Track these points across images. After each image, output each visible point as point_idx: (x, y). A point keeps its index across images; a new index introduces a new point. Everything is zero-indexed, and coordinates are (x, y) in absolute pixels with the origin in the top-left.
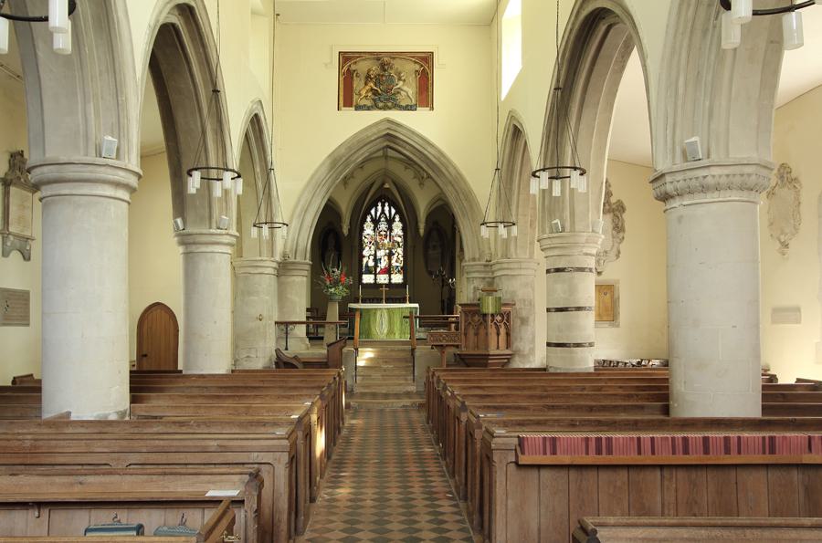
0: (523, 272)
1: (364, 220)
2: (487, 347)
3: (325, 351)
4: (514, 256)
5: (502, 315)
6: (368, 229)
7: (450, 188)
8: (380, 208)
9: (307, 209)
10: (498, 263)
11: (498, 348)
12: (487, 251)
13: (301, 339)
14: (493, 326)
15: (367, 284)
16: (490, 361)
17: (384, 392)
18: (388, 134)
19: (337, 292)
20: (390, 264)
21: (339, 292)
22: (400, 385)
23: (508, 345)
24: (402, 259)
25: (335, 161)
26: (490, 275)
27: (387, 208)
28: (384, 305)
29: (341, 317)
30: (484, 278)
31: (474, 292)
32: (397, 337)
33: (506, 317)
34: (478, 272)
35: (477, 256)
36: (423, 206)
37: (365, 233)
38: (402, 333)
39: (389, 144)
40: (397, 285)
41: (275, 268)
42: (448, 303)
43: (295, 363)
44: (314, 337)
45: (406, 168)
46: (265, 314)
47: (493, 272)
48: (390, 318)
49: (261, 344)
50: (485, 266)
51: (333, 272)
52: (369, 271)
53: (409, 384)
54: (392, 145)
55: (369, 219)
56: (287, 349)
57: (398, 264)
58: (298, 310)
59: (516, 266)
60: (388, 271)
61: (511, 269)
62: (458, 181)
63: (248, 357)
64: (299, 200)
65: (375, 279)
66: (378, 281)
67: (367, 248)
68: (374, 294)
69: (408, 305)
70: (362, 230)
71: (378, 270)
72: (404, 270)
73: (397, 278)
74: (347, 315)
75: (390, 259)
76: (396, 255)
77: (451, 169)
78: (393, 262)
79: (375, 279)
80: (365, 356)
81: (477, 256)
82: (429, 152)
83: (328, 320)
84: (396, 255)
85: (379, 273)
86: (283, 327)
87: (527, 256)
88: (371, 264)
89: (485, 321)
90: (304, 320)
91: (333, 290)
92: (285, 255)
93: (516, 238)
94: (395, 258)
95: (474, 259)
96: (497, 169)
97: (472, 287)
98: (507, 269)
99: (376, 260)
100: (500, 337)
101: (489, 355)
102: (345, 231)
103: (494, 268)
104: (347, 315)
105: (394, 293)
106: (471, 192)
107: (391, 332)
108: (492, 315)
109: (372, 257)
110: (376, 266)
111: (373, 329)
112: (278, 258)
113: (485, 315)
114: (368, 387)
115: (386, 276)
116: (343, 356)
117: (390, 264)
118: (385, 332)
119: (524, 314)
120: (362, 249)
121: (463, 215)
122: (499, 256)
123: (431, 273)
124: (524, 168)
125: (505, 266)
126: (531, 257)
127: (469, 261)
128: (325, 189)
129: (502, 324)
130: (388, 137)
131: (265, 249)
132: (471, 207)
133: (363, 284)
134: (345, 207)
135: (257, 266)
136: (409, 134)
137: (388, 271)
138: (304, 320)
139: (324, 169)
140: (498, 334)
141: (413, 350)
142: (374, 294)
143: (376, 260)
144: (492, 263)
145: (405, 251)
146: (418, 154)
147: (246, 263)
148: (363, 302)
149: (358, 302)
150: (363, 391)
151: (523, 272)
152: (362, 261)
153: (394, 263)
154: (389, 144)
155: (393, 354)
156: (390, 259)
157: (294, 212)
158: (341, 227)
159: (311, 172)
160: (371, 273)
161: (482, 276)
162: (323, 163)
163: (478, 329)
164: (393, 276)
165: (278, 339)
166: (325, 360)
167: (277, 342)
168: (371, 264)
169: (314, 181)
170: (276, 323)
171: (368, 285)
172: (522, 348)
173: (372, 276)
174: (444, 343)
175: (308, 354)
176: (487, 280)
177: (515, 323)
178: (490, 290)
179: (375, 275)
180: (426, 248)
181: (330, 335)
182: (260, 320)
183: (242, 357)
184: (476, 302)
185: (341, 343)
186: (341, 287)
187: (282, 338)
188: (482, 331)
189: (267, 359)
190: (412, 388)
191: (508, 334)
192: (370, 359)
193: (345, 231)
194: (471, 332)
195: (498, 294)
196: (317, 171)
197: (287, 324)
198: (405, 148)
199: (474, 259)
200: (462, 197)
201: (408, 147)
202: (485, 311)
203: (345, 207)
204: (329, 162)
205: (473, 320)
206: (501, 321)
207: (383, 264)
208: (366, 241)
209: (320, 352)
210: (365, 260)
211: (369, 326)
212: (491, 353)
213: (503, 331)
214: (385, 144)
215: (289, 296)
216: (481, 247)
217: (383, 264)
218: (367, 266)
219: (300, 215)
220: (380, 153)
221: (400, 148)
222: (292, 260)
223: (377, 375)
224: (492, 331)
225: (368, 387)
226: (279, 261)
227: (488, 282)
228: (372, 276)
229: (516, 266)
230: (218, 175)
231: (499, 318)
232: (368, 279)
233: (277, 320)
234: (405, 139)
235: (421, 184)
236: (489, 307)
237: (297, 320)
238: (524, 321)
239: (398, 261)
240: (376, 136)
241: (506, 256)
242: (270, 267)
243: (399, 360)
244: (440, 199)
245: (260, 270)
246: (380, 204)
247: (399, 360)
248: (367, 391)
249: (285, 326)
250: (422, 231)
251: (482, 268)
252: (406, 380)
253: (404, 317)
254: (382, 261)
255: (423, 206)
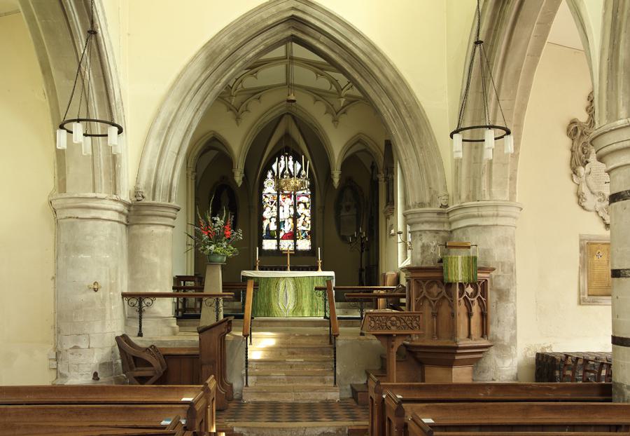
0: (500, 221)
1: (264, 177)
2: (453, 333)
3: (197, 339)
4: (488, 198)
5: (474, 285)
6: (269, 188)
7: (386, 100)
8: (282, 162)
9: (171, 125)
10: (461, 208)
11: (469, 336)
12: (441, 193)
13: (164, 320)
14: (462, 302)
15: (268, 251)
16: (457, 358)
17: (290, 401)
18: (293, 18)
19: (218, 250)
20: (295, 228)
21: (223, 251)
22: (314, 390)
23: (484, 332)
24: (309, 222)
25: (215, 56)
26: (446, 227)
27: (291, 163)
28: (289, 274)
29: (226, 287)
30: (437, 232)
31: (423, 252)
32: (307, 315)
33: (481, 288)
34: (427, 222)
35: (427, 199)
36: (337, 148)
37: (265, 192)
38: (314, 310)
39: (294, 33)
40: (304, 253)
41: (121, 213)
42: (369, 271)
43: (147, 357)
44: (185, 314)
45: (316, 100)
46: (103, 281)
47: (450, 223)
48: (296, 287)
49: (97, 328)
50: (439, 213)
51: (215, 222)
52: (270, 236)
53: (328, 389)
54: (300, 35)
55: (270, 175)
56: (140, 335)
57: (304, 228)
58: (158, 275)
59: (490, 211)
60: (293, 236)
61: (482, 216)
62: (397, 90)
63: (75, 347)
64: (159, 112)
65: (278, 245)
66: (282, 248)
67: (268, 209)
68: (277, 260)
69: (320, 273)
70: (262, 187)
71: (282, 234)
72: (312, 235)
73: (304, 245)
74: (235, 286)
75: (295, 222)
76: (303, 217)
77: (387, 71)
78: (299, 225)
79: (278, 245)
80: (261, 345)
81: (427, 199)
82: (355, 45)
83: (206, 291)
84: (303, 217)
85: (282, 239)
86: (134, 301)
87: (507, 197)
88: (273, 227)
89: (451, 295)
90: (170, 290)
91: (212, 247)
92: (137, 193)
93: (491, 162)
94: (300, 221)
95: (422, 205)
96: (478, 43)
97: (420, 244)
98: (478, 216)
99: (279, 224)
100: (472, 320)
101: (457, 348)
102: (238, 178)
103: (452, 216)
104: (235, 286)
105: (302, 261)
106: (416, 105)
107: (298, 307)
108: (461, 285)
109: (274, 220)
110: (279, 230)
111: (274, 304)
112: (125, 196)
113: (450, 285)
114: (265, 393)
115: (291, 242)
116: (227, 347)
117: (295, 228)
118: (291, 307)
119: (503, 283)
120: (262, 210)
121: (405, 139)
122: (464, 196)
123: (344, 238)
124: (509, 55)
125: (474, 212)
126: (512, 198)
127: (414, 207)
128: (198, 97)
129: (475, 300)
130: (293, 23)
131: (103, 180)
132: (417, 127)
133: (262, 251)
134: (237, 141)
135: (89, 208)
136: (324, 17)
137: (293, 236)
138: (170, 290)
139: (198, 66)
140: (469, 315)
141: (332, 338)
142: (277, 260)
143: (279, 224)
144: (451, 207)
145: (313, 213)
146: (338, 49)
147: (71, 202)
148: (262, 269)
149: (254, 269)
150: (259, 399)
151: (500, 221)
152: (262, 224)
153: (300, 227)
154: (294, 33)
155: (303, 341)
156: (295, 222)
157: (150, 130)
158: (233, 174)
159: (177, 70)
160: (272, 238)
161: (435, 228)
162: (195, 57)
163: (438, 306)
164: (292, 248)
165: (127, 319)
166: (198, 352)
167: (126, 325)
168: (273, 227)
169: (181, 83)
170: (124, 295)
171: (270, 252)
172: (500, 336)
173: (275, 242)
174: (394, 331)
175: (174, 342)
176: (442, 234)
177: (492, 296)
178: (449, 244)
179: (278, 240)
180: (338, 209)
181: (208, 317)
182: (96, 290)
183: (65, 347)
184: (438, 265)
185: (223, 328)
186: (225, 244)
187: (134, 318)
188: (444, 310)
189: (107, 350)
190: (334, 395)
191: (484, 316)
192: (271, 349)
193: (238, 178)
194: (427, 311)
195: (471, 252)
196: (187, 67)
197: (141, 297)
198: (318, 40)
199: (422, 205)
200: (403, 111)
201: (323, 38)
202: (452, 278)
203: (237, 141)
204: (202, 56)
205: (429, 293)
206: (474, 295)
207: (287, 228)
208: (267, 200)
209: (189, 338)
210: (265, 223)
211: (269, 300)
212: (461, 344)
213: (476, 309)
214: (289, 33)
215: (144, 255)
216: (433, 185)
217: (287, 228)
218: (268, 229)
219: (160, 135)
220: (280, 52)
221: (314, 42)
222: (148, 200)
223: (279, 374)
224: (461, 309)
225: (265, 393)
226: (128, 200)
227: (443, 237)
228: (275, 242)
229: (490, 211)
230: (103, 129)
231: (470, 290)
232: (269, 245)
233: (125, 291)
234: (318, 24)
235: (335, 121)
236: (458, 274)
237: (157, 291)
238: (503, 295)
239: (304, 225)
240: (274, 20)
241: (473, 196)
242: (111, 210)
243: (314, 350)
244: (359, 141)
245: (93, 214)
246: (282, 158)
247: (314, 350)
248: (263, 399)
249: (138, 301)
250: (336, 180)
251: (435, 217)
252: (323, 381)
253: (316, 289)
254: (286, 224)
255: (337, 148)
